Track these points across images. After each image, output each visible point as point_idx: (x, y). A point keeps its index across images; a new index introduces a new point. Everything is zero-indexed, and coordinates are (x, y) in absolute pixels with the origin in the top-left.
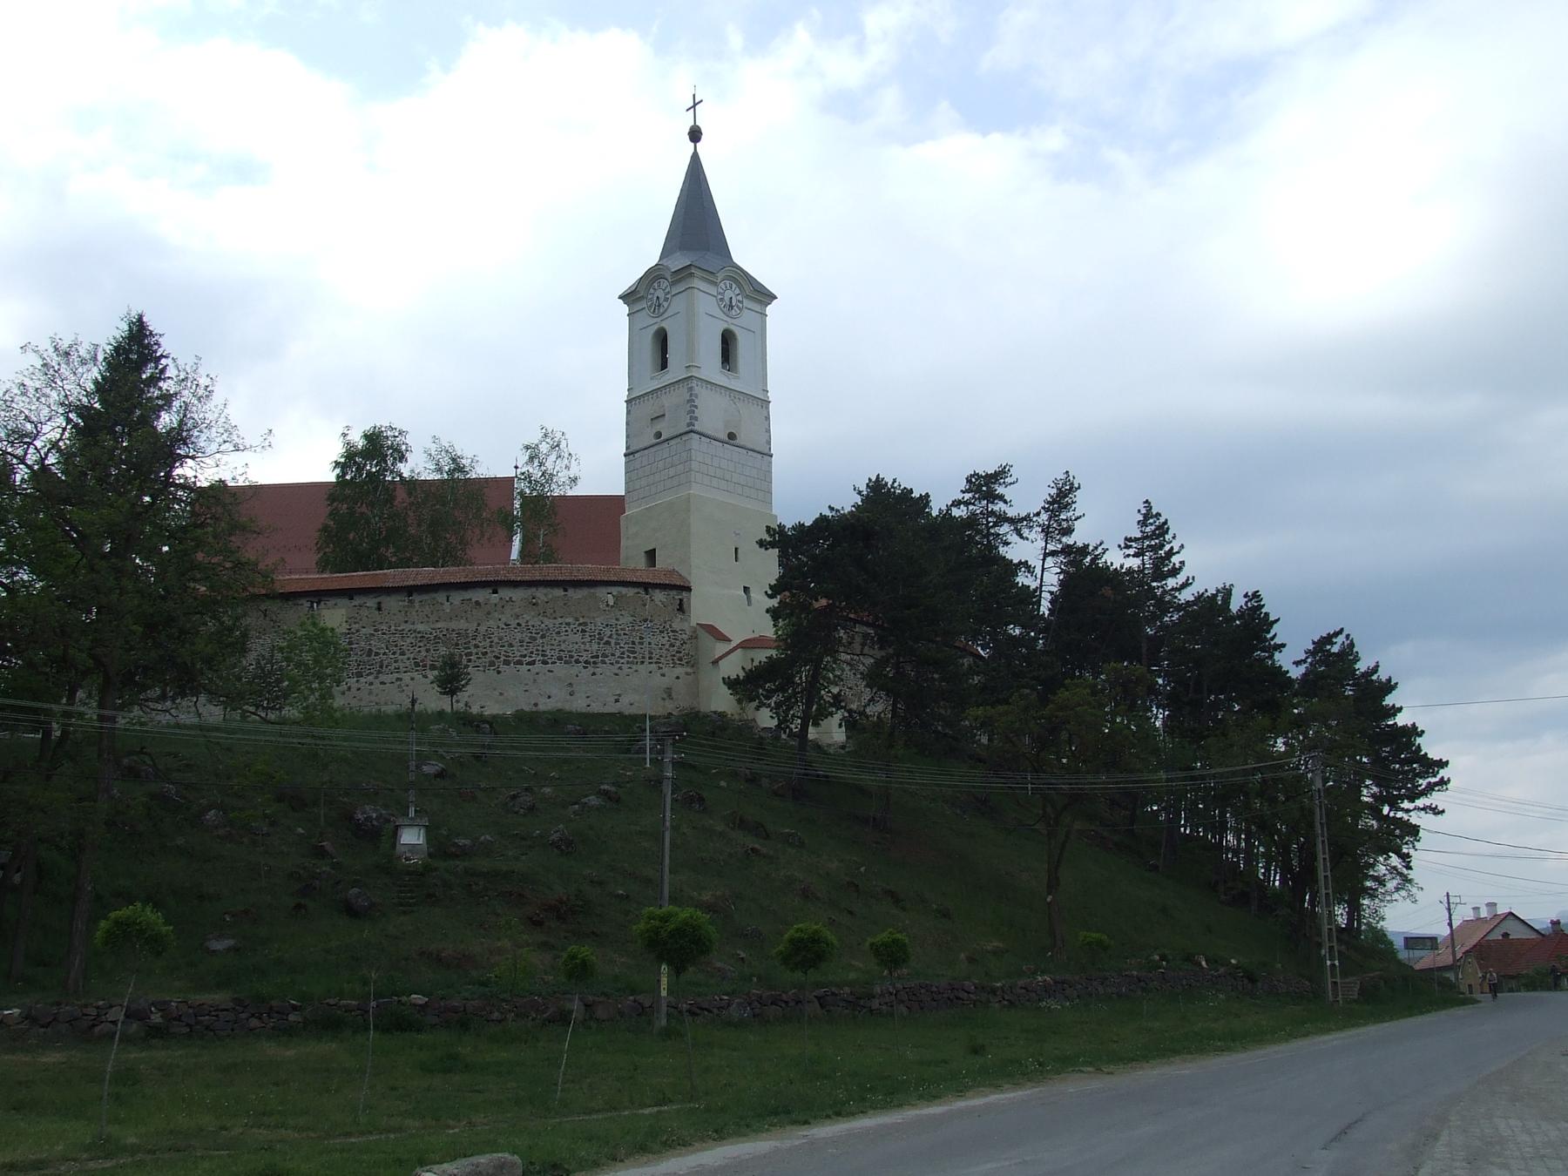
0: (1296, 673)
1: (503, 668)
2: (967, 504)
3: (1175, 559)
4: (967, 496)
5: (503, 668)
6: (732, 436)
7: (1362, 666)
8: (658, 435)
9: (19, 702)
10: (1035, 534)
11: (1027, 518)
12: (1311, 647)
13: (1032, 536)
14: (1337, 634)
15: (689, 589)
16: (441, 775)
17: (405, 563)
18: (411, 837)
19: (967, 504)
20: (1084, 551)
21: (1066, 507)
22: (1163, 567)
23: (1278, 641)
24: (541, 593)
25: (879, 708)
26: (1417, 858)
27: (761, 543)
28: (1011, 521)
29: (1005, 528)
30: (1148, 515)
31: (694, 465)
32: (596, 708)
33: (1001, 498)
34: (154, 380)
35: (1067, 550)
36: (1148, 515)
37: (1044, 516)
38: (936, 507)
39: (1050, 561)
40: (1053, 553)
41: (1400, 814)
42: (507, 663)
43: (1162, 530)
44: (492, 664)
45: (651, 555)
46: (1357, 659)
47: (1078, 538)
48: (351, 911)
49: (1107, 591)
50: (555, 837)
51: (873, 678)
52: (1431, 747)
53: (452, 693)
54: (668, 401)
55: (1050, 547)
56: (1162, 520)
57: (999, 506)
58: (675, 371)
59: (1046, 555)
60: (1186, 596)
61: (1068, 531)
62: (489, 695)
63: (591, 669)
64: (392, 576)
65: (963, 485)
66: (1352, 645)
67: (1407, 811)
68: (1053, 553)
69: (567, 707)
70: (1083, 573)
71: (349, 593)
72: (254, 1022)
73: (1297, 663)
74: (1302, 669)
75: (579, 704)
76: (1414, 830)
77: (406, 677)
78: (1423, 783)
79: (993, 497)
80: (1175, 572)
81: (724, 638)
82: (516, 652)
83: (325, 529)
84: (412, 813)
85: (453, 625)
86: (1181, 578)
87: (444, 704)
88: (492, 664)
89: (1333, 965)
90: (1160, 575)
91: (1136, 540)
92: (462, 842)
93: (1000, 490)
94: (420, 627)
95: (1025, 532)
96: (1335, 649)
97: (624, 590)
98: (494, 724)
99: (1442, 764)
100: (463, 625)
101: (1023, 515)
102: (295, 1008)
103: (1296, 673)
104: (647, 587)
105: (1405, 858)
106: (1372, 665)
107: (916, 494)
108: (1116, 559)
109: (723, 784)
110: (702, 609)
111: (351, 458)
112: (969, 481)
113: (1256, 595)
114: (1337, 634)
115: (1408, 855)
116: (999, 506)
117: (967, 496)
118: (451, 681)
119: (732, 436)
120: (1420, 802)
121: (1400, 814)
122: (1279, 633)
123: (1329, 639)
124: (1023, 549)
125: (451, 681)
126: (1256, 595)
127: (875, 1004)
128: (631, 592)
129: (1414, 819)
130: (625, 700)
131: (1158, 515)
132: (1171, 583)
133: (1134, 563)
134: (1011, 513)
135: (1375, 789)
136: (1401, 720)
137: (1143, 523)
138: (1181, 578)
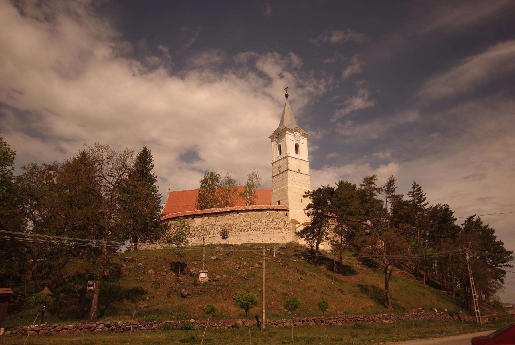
0: (463, 227)
1: (240, 232)
2: (364, 185)
3: (423, 197)
4: (364, 183)
5: (240, 232)
6: (299, 171)
7: (483, 225)
8: (280, 171)
9: (79, 239)
10: (384, 192)
11: (381, 188)
12: (466, 220)
13: (383, 193)
14: (475, 215)
15: (288, 210)
16: (216, 260)
17: (217, 207)
18: (203, 276)
19: (364, 185)
20: (397, 196)
21: (392, 185)
22: (420, 199)
23: (455, 218)
24: (249, 213)
25: (338, 239)
26: (505, 279)
27: (303, 196)
28: (376, 189)
29: (375, 192)
30: (415, 185)
31: (289, 178)
32: (265, 242)
33: (373, 183)
34: (149, 163)
35: (393, 196)
36: (415, 185)
37: (386, 188)
38: (456, 223)
39: (388, 199)
40: (389, 197)
41: (499, 267)
42: (241, 231)
43: (420, 189)
44: (237, 231)
45: (279, 202)
46: (482, 223)
47: (397, 193)
48: (183, 296)
49: (406, 207)
50: (243, 275)
51: (335, 231)
52: (507, 247)
53: (225, 239)
54: (281, 163)
55: (388, 196)
56: (419, 187)
57: (373, 186)
58: (283, 155)
59: (387, 198)
60: (427, 207)
61: (393, 191)
62: (234, 240)
63: (263, 232)
64: (213, 210)
65: (363, 180)
66: (480, 219)
67: (501, 266)
68: (389, 197)
69: (257, 242)
70: (398, 204)
71: (201, 215)
72: (143, 328)
73: (462, 225)
74: (464, 226)
75: (260, 241)
76: (504, 272)
77: (216, 236)
78: (505, 258)
79: (371, 183)
80: (424, 201)
81: (299, 223)
82: (244, 228)
83: (35, 167)
84: (204, 269)
85: (228, 222)
86: (425, 202)
87: (223, 242)
88: (237, 231)
89: (478, 312)
90: (420, 202)
91: (412, 192)
92: (218, 277)
93: (373, 181)
94: (219, 223)
95: (381, 192)
96: (474, 220)
97: (271, 211)
98: (235, 247)
99: (511, 252)
100: (230, 222)
101: (380, 187)
102: (155, 323)
103: (463, 227)
104: (277, 210)
105: (502, 281)
106: (486, 225)
107: (352, 185)
108: (406, 198)
109: (295, 261)
110: (292, 215)
111: (204, 182)
112: (364, 179)
113: (447, 205)
114: (475, 215)
115: (502, 280)
116: (373, 186)
117: (364, 183)
118: (225, 235)
119: (299, 171)
120: (505, 264)
121: (499, 267)
122: (454, 216)
123: (472, 217)
124: (381, 197)
125: (225, 235)
126: (447, 205)
127: (332, 321)
128: (273, 212)
129: (504, 268)
130: (272, 240)
131: (418, 185)
132: (423, 203)
133: (412, 198)
134: (376, 187)
135: (491, 261)
136: (497, 240)
137: (414, 187)
138: (425, 202)
